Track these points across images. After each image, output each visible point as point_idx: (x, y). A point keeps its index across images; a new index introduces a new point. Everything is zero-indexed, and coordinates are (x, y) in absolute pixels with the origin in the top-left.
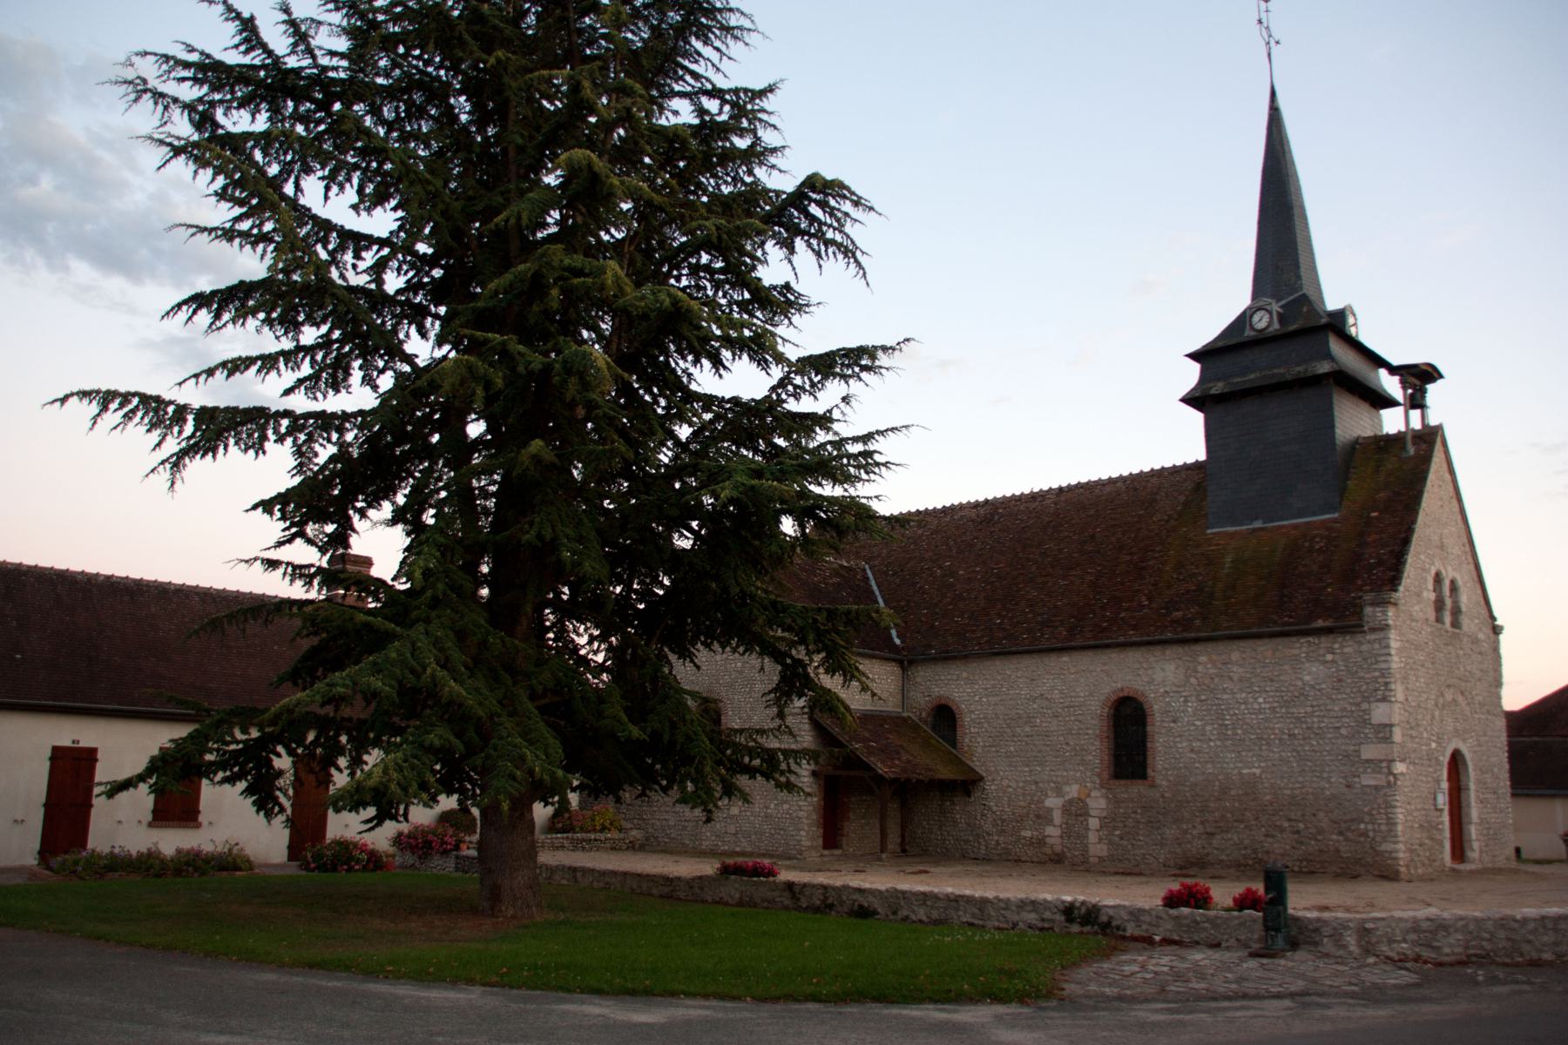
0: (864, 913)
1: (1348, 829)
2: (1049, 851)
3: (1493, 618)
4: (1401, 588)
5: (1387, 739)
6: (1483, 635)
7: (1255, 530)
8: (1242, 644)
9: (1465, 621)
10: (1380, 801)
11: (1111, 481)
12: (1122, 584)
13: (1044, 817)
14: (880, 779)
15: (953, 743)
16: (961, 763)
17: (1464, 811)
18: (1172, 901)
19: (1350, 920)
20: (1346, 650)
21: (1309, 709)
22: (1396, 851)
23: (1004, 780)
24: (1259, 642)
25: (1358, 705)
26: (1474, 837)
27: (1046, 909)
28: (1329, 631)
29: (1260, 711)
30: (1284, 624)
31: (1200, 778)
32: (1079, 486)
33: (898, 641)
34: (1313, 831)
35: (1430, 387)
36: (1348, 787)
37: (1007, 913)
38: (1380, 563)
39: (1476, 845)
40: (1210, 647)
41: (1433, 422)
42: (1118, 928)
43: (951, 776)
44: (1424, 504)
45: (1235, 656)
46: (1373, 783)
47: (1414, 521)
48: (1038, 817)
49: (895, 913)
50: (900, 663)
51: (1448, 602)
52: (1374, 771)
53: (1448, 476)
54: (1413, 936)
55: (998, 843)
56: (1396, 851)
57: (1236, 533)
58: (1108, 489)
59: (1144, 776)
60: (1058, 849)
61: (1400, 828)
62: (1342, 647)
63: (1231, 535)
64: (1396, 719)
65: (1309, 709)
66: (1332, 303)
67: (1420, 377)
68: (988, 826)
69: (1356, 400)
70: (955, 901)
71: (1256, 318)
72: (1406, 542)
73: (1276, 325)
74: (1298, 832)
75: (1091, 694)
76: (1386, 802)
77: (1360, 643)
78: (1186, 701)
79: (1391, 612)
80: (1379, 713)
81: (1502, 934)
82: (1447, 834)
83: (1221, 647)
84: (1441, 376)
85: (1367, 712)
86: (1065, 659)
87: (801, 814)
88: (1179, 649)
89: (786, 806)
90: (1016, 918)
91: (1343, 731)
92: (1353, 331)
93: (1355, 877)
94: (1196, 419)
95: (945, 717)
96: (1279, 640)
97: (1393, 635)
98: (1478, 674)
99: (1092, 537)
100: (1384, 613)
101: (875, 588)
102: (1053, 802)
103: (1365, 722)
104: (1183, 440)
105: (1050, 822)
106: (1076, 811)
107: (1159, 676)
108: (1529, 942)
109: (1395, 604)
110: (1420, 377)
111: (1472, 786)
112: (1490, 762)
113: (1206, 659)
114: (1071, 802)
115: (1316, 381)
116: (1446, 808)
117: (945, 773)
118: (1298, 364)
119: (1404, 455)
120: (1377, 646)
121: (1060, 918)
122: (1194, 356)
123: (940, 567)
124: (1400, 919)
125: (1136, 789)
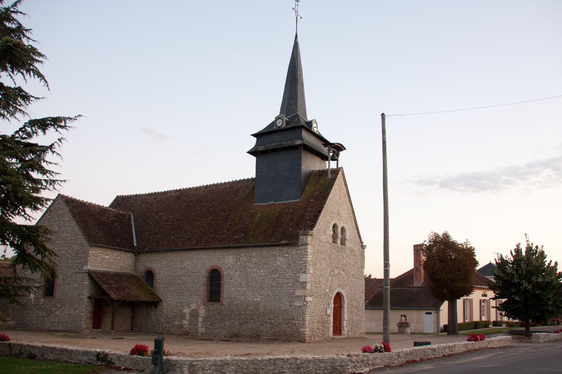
0: (32, 357)
1: (289, 322)
2: (184, 330)
3: (362, 242)
4: (315, 229)
5: (305, 288)
6: (357, 248)
7: (270, 205)
8: (257, 249)
9: (348, 243)
10: (301, 312)
11: (225, 183)
12: (220, 224)
13: (183, 317)
14: (112, 300)
15: (152, 286)
16: (155, 294)
17: (342, 315)
18: (133, 352)
19: (186, 361)
20: (293, 253)
21: (278, 276)
22: (305, 331)
23: (169, 301)
24: (262, 249)
25: (296, 274)
26: (345, 325)
27: (91, 355)
28: (287, 245)
29: (261, 276)
30: (273, 242)
31: (239, 302)
32: (214, 185)
33: (135, 244)
34: (277, 323)
35: (341, 153)
36: (290, 306)
37: (78, 357)
38: (310, 219)
39: (346, 329)
40: (245, 250)
41: (339, 166)
42: (113, 363)
43: (146, 299)
44: (329, 197)
45: (254, 254)
46: (298, 305)
47: (324, 204)
48: (181, 316)
49: (43, 356)
50: (134, 253)
51: (340, 235)
52: (299, 300)
53: (344, 187)
54: (214, 368)
55: (166, 327)
56: (305, 331)
57: (264, 205)
58: (223, 186)
59: (218, 300)
60: (187, 329)
61: (307, 322)
62: (291, 251)
63: (261, 206)
64: (308, 280)
65: (278, 276)
66: (309, 119)
67: (339, 148)
68: (163, 320)
69: (311, 155)
70: (63, 351)
71: (278, 122)
72: (320, 211)
73: (285, 125)
74: (272, 324)
75: (202, 268)
76: (303, 312)
77: (298, 250)
78: (235, 271)
79: (309, 238)
80: (302, 278)
81: (252, 366)
82: (332, 324)
83: (249, 250)
84: (345, 149)
85: (298, 277)
86: (194, 253)
87: (82, 314)
88: (235, 251)
89: (77, 311)
90: (81, 358)
91: (290, 284)
92: (315, 130)
93: (290, 341)
94: (253, 159)
95: (150, 275)
96: (269, 248)
97: (309, 247)
98: (353, 263)
99: (213, 205)
100: (307, 238)
101: (133, 223)
102: (186, 311)
103: (298, 281)
104: (246, 169)
105: (185, 319)
106: (194, 314)
107: (227, 260)
108: (263, 369)
109: (311, 235)
110: (339, 148)
111: (346, 306)
112: (355, 297)
113: (244, 254)
114: (193, 310)
115: (296, 147)
116: (332, 314)
117: (144, 298)
118: (290, 140)
119: (327, 178)
120: (303, 251)
121: (95, 358)
122: (254, 135)
123: (158, 215)
124: (209, 361)
125: (216, 306)
